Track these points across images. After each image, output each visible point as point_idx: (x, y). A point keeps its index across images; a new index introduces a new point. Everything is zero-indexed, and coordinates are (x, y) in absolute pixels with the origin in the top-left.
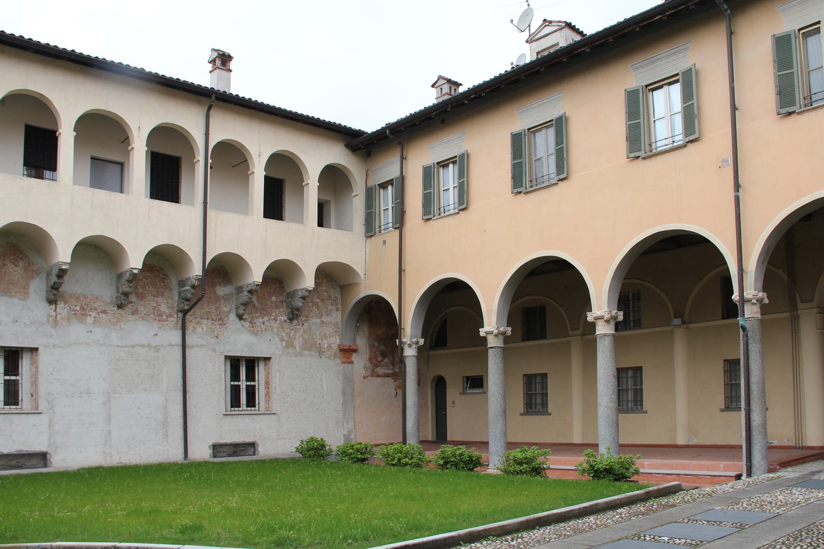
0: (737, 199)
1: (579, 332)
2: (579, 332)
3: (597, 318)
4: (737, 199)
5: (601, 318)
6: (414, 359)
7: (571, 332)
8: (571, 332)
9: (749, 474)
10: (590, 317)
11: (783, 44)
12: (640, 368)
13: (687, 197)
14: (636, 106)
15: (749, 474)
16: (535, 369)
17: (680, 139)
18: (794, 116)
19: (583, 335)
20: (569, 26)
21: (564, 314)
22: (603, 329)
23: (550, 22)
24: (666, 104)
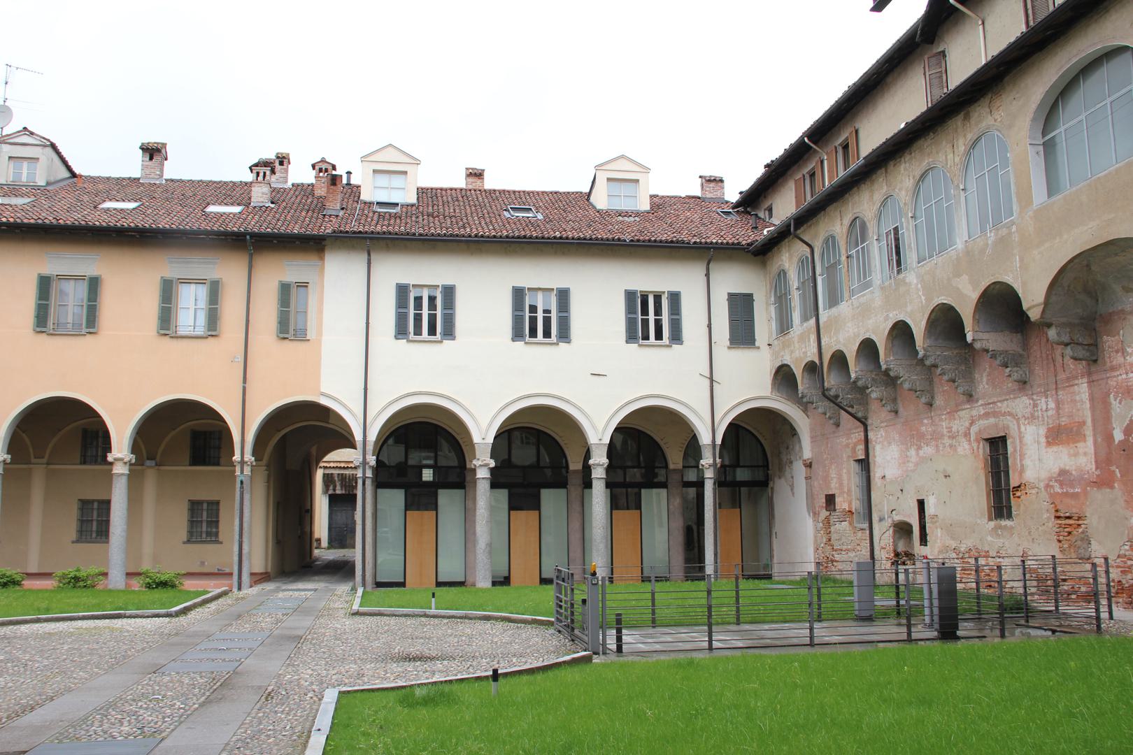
0: (244, 389)
1: (45, 460)
2: (45, 460)
3: (116, 459)
4: (244, 389)
5: (121, 460)
6: (124, 480)
7: (33, 460)
8: (33, 460)
9: (240, 589)
10: (110, 458)
11: (285, 289)
12: (218, 503)
13: (205, 376)
14: (168, 292)
15: (240, 589)
16: (204, 495)
17: (200, 331)
18: (286, 342)
19: (48, 464)
20: (53, 146)
21: (27, 440)
22: (119, 469)
23: (32, 133)
24: (191, 302)
